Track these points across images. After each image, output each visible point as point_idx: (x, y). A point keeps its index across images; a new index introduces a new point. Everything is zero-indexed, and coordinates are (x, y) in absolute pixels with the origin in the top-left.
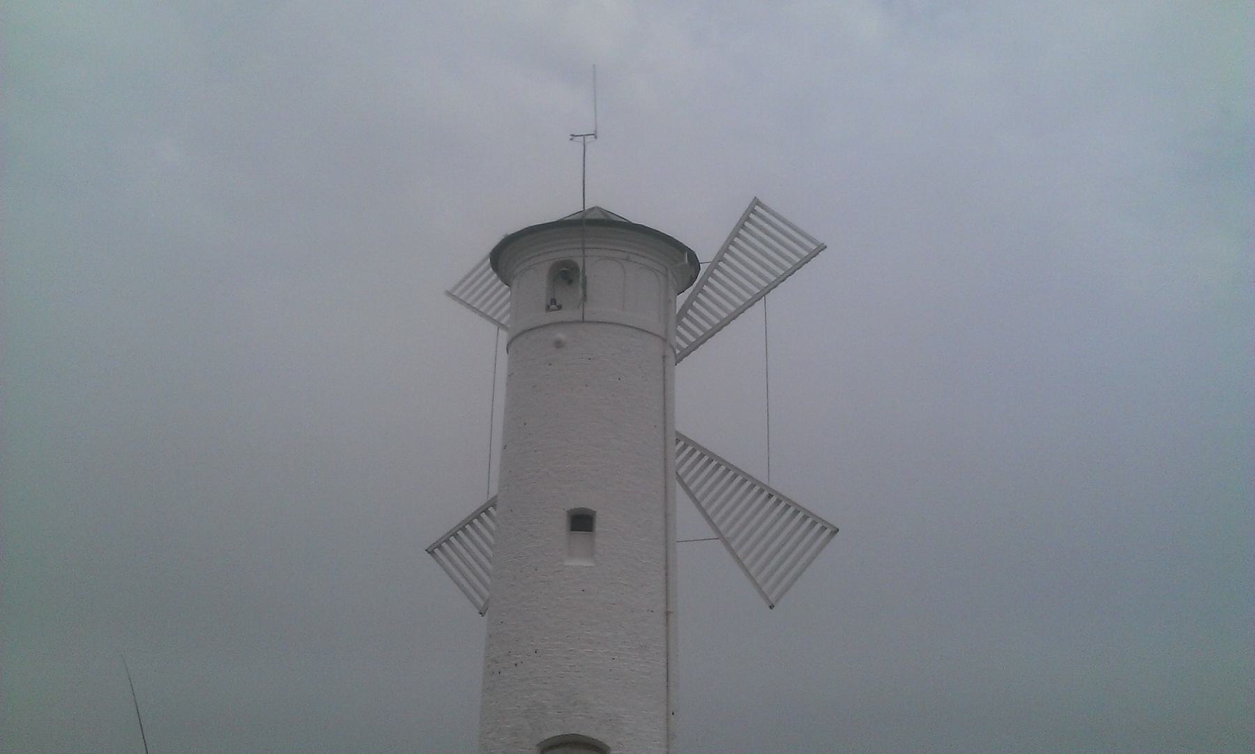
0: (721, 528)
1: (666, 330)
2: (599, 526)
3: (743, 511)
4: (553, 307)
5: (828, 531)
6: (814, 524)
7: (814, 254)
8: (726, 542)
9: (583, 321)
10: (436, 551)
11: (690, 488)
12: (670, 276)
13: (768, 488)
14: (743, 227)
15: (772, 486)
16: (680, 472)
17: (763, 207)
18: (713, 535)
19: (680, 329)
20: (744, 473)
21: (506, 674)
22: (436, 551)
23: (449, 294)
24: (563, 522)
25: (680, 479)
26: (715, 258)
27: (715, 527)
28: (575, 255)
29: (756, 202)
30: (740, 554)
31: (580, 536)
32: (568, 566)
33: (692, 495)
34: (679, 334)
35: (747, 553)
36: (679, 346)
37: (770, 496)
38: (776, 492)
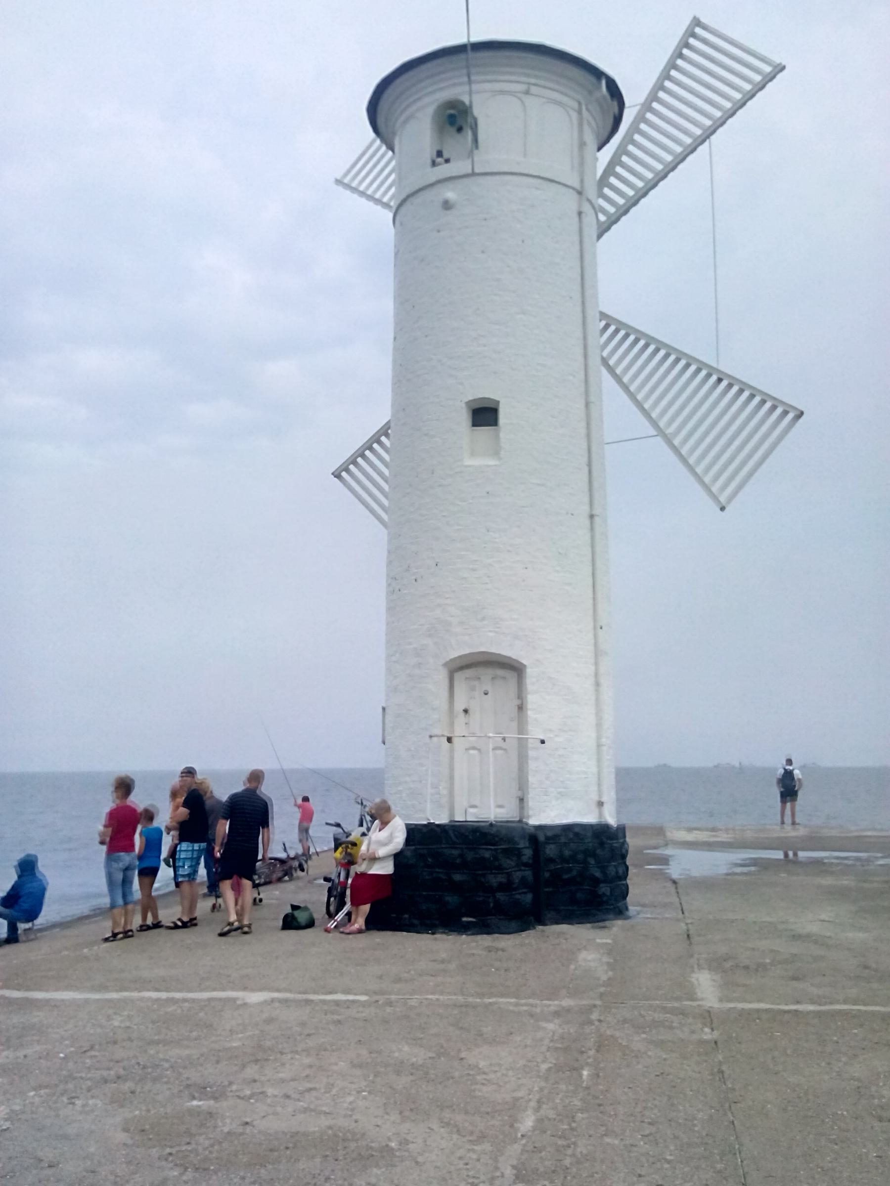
0: (662, 424)
1: (582, 181)
2: (502, 419)
4: (439, 160)
5: (791, 416)
7: (771, 77)
8: (669, 441)
9: (473, 174)
10: (344, 474)
11: (690, 462)
12: (585, 113)
13: (718, 371)
14: (681, 56)
15: (722, 368)
17: (705, 28)
18: (653, 432)
21: (405, 592)
22: (344, 474)
23: (339, 182)
24: (465, 418)
25: (605, 362)
26: (647, 99)
27: (654, 423)
28: (457, 91)
29: (697, 22)
30: (684, 451)
31: (484, 432)
32: (470, 466)
33: (618, 379)
35: (648, 396)
36: (604, 212)
37: (720, 380)
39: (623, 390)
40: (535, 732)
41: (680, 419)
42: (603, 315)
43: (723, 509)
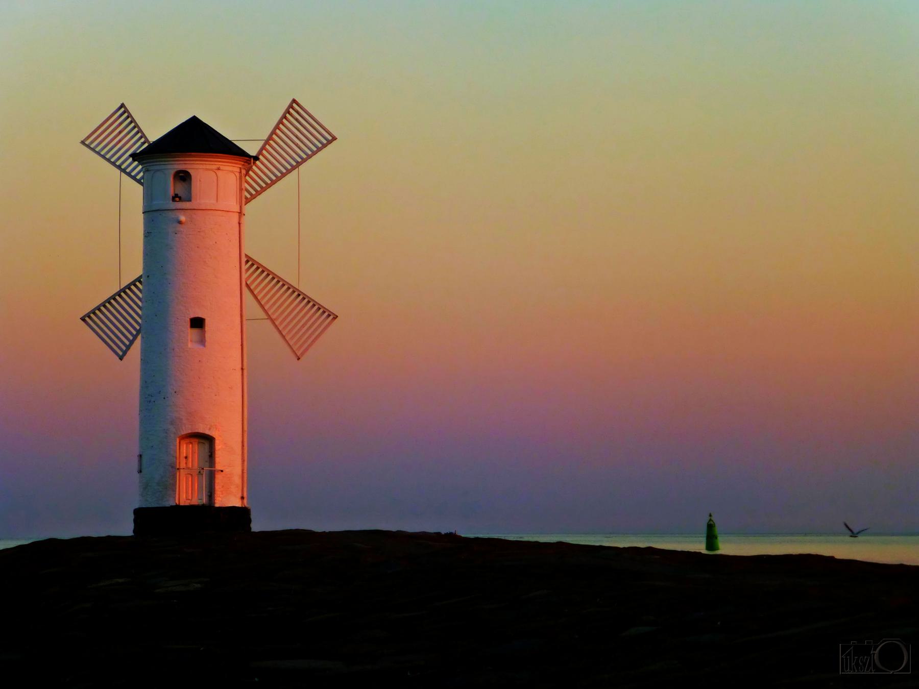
3: (303, 317)
6: (258, 268)
8: (273, 321)
13: (298, 290)
15: (302, 289)
16: (248, 283)
19: (248, 178)
20: (268, 270)
25: (248, 286)
27: (266, 312)
29: (294, 101)
34: (247, 182)
35: (260, 292)
37: (299, 295)
38: (288, 283)
39: (408, 532)
40: (218, 467)
41: (269, 295)
42: (246, 256)
43: (299, 359)
